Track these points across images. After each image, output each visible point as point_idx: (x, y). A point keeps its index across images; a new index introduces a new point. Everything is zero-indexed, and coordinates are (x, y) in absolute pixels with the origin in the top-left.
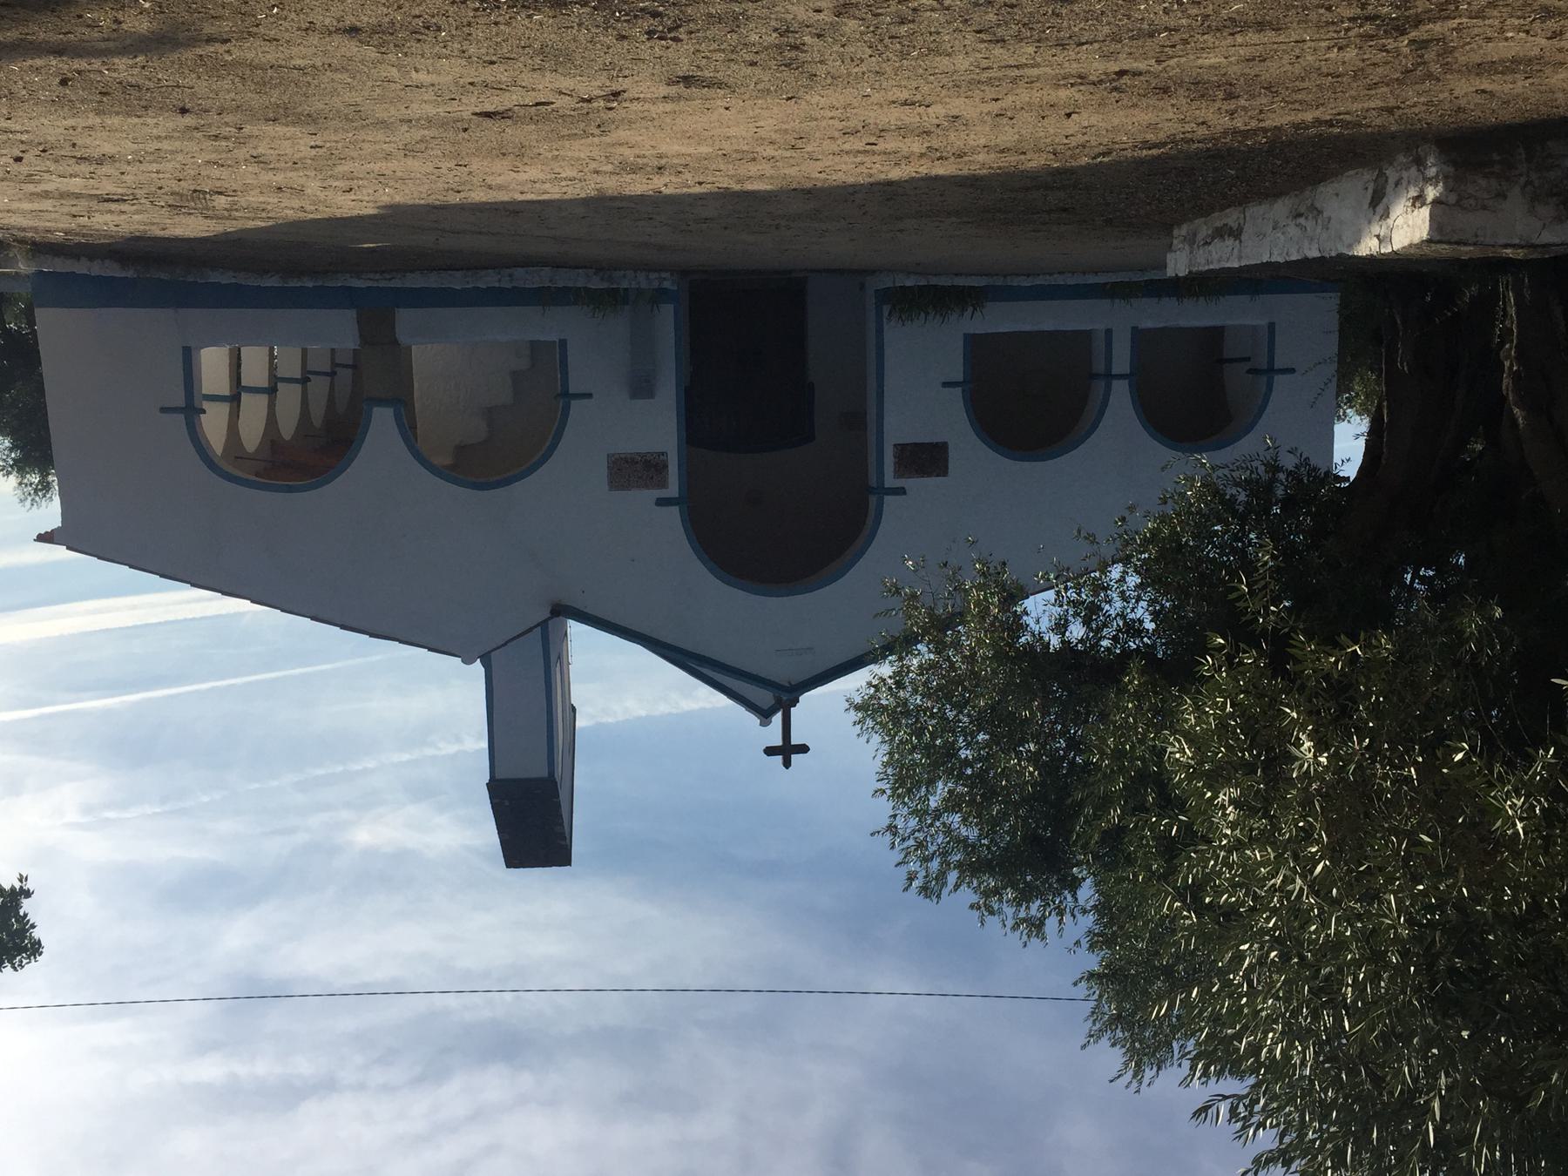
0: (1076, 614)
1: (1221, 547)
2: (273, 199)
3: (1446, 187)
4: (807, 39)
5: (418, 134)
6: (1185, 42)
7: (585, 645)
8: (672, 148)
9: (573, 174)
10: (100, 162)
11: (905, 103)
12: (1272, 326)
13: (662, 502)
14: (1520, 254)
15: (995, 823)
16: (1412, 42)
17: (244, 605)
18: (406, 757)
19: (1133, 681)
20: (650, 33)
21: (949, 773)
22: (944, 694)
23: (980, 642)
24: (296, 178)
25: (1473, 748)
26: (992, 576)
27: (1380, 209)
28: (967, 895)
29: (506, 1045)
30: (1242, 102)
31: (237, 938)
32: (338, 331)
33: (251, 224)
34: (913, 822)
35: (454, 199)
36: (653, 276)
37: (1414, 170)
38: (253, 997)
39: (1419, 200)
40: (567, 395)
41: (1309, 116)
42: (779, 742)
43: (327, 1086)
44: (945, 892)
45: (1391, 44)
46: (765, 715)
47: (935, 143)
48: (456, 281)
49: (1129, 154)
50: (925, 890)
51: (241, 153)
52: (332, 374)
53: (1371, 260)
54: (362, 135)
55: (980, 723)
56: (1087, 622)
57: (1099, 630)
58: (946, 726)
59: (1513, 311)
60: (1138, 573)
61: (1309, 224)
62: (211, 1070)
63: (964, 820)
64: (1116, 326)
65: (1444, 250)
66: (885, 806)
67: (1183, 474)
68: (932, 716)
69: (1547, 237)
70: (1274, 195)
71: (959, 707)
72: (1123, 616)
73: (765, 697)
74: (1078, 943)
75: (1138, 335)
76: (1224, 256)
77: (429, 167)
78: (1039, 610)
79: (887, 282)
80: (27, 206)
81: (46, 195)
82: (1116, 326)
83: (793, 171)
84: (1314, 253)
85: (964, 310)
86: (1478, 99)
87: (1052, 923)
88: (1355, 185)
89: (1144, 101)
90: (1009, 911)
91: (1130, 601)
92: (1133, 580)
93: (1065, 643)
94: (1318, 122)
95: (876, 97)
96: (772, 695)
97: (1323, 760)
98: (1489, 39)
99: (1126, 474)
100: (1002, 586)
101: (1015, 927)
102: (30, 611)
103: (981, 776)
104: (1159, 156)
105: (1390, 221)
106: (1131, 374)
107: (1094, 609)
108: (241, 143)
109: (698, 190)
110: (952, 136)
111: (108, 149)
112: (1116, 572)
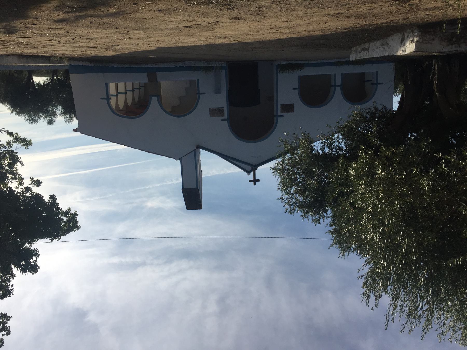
0: (326, 146)
1: (363, 129)
2: (130, 47)
3: (419, 38)
4: (264, 9)
5: (169, 32)
6: (354, 6)
7: (204, 155)
8: (229, 33)
9: (203, 39)
10: (92, 39)
11: (286, 21)
12: (377, 72)
13: (223, 120)
14: (438, 54)
15: (307, 197)
16: (408, 5)
17: (123, 147)
18: (159, 185)
19: (341, 160)
20: (228, 9)
21: (295, 185)
22: (294, 166)
23: (303, 153)
24: (137, 42)
25: (417, 170)
26: (305, 137)
27: (403, 43)
28: (300, 213)
29: (187, 254)
30: (368, 19)
31: (120, 229)
32: (143, 78)
33: (123, 52)
34: (287, 196)
35: (174, 46)
36: (220, 63)
37: (411, 34)
38: (125, 242)
39: (412, 41)
40: (199, 93)
41: (385, 21)
42: (253, 179)
43: (143, 264)
44: (295, 212)
45: (403, 5)
46: (249, 173)
47: (293, 30)
48: (171, 65)
49: (340, 31)
50: (290, 212)
51: (127, 36)
52: (140, 89)
53: (401, 56)
54: (156, 32)
55: (303, 173)
56: (329, 148)
57: (332, 149)
58: (295, 174)
59: (436, 68)
60: (342, 135)
61: (386, 47)
62: (116, 260)
63: (299, 196)
64: (337, 73)
65: (419, 53)
66: (279, 193)
67: (354, 110)
68: (291, 171)
69: (445, 50)
70: (376, 40)
71: (298, 169)
72: (338, 146)
73: (249, 168)
74: (327, 225)
75: (344, 76)
76: (365, 55)
77: (170, 39)
78: (318, 145)
79: (279, 63)
80: (71, 49)
81: (76, 47)
82: (337, 73)
83: (257, 37)
84: (386, 55)
85: (298, 70)
86: (427, 16)
87: (321, 220)
88: (397, 37)
89: (344, 19)
90: (310, 217)
91: (340, 141)
92: (341, 137)
93: (324, 153)
94: (387, 22)
95: (279, 20)
96: (250, 167)
97: (383, 174)
98: (428, 3)
99: (340, 110)
100: (308, 139)
101: (313, 221)
102: (68, 149)
103: (303, 185)
104: (348, 31)
105: (405, 46)
106: (341, 85)
107: (331, 144)
108: (127, 34)
109: (234, 42)
110: (297, 28)
111: (96, 36)
112: (336, 135)
